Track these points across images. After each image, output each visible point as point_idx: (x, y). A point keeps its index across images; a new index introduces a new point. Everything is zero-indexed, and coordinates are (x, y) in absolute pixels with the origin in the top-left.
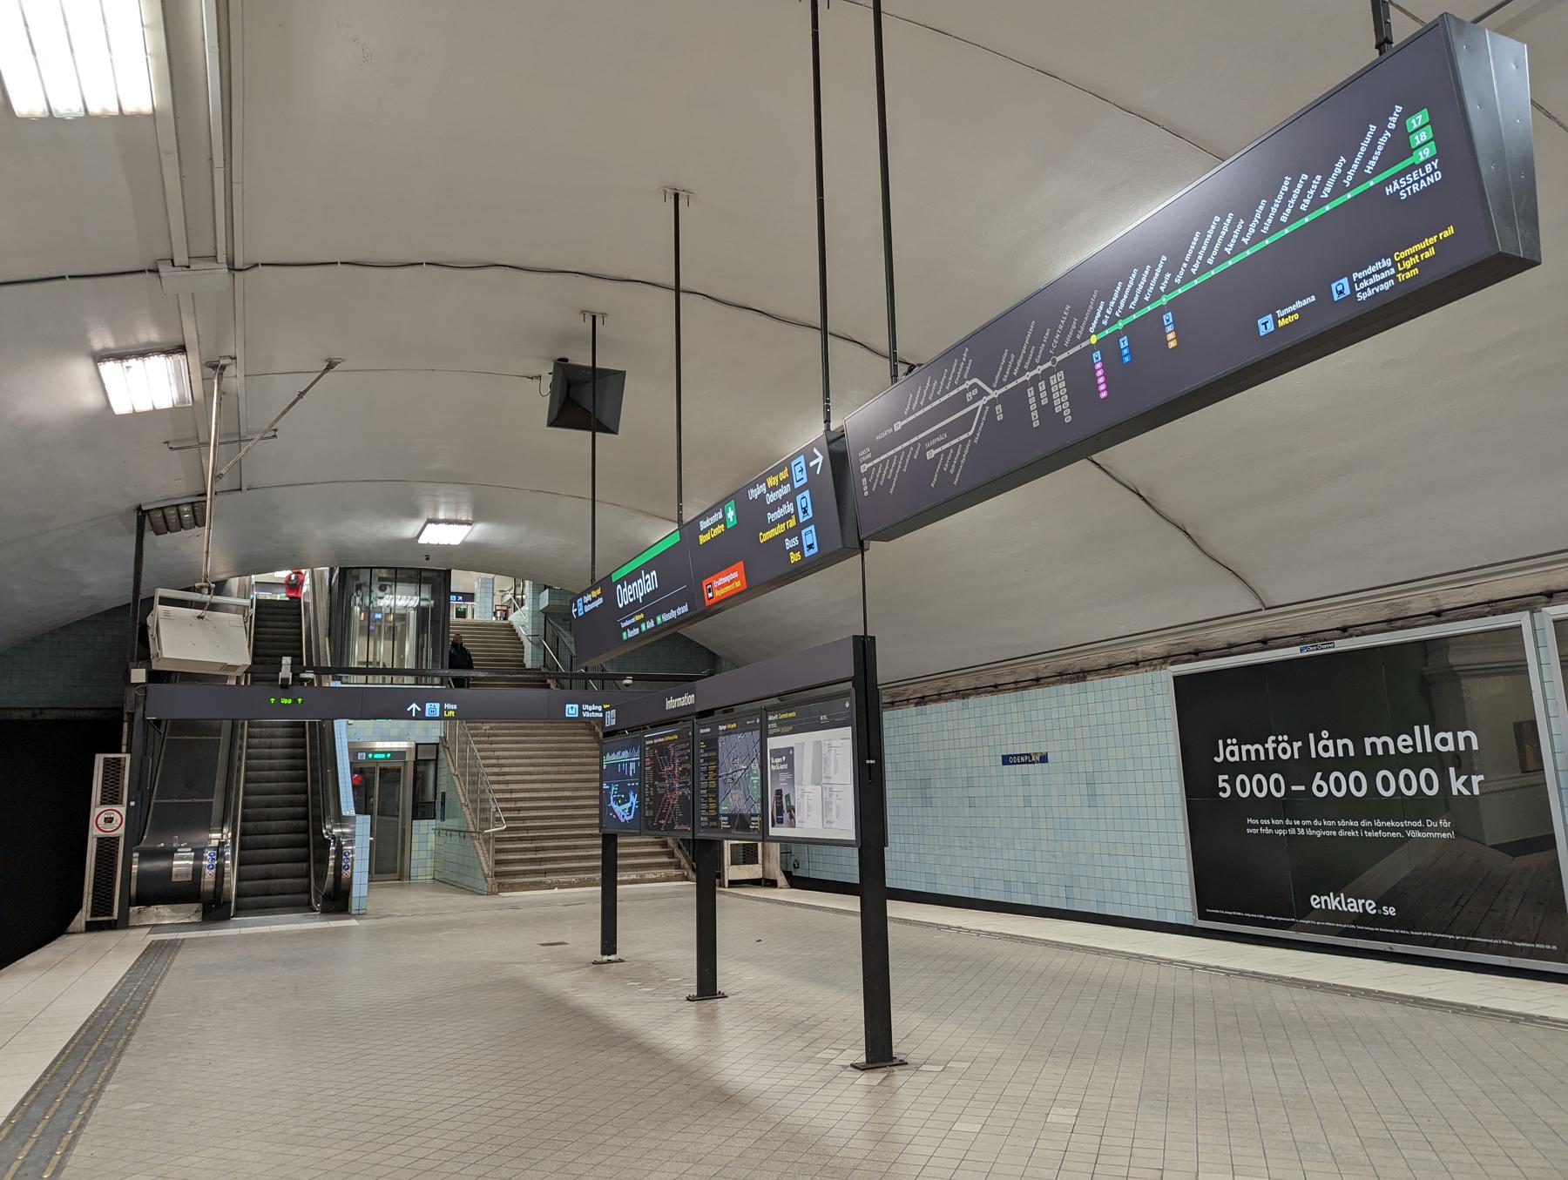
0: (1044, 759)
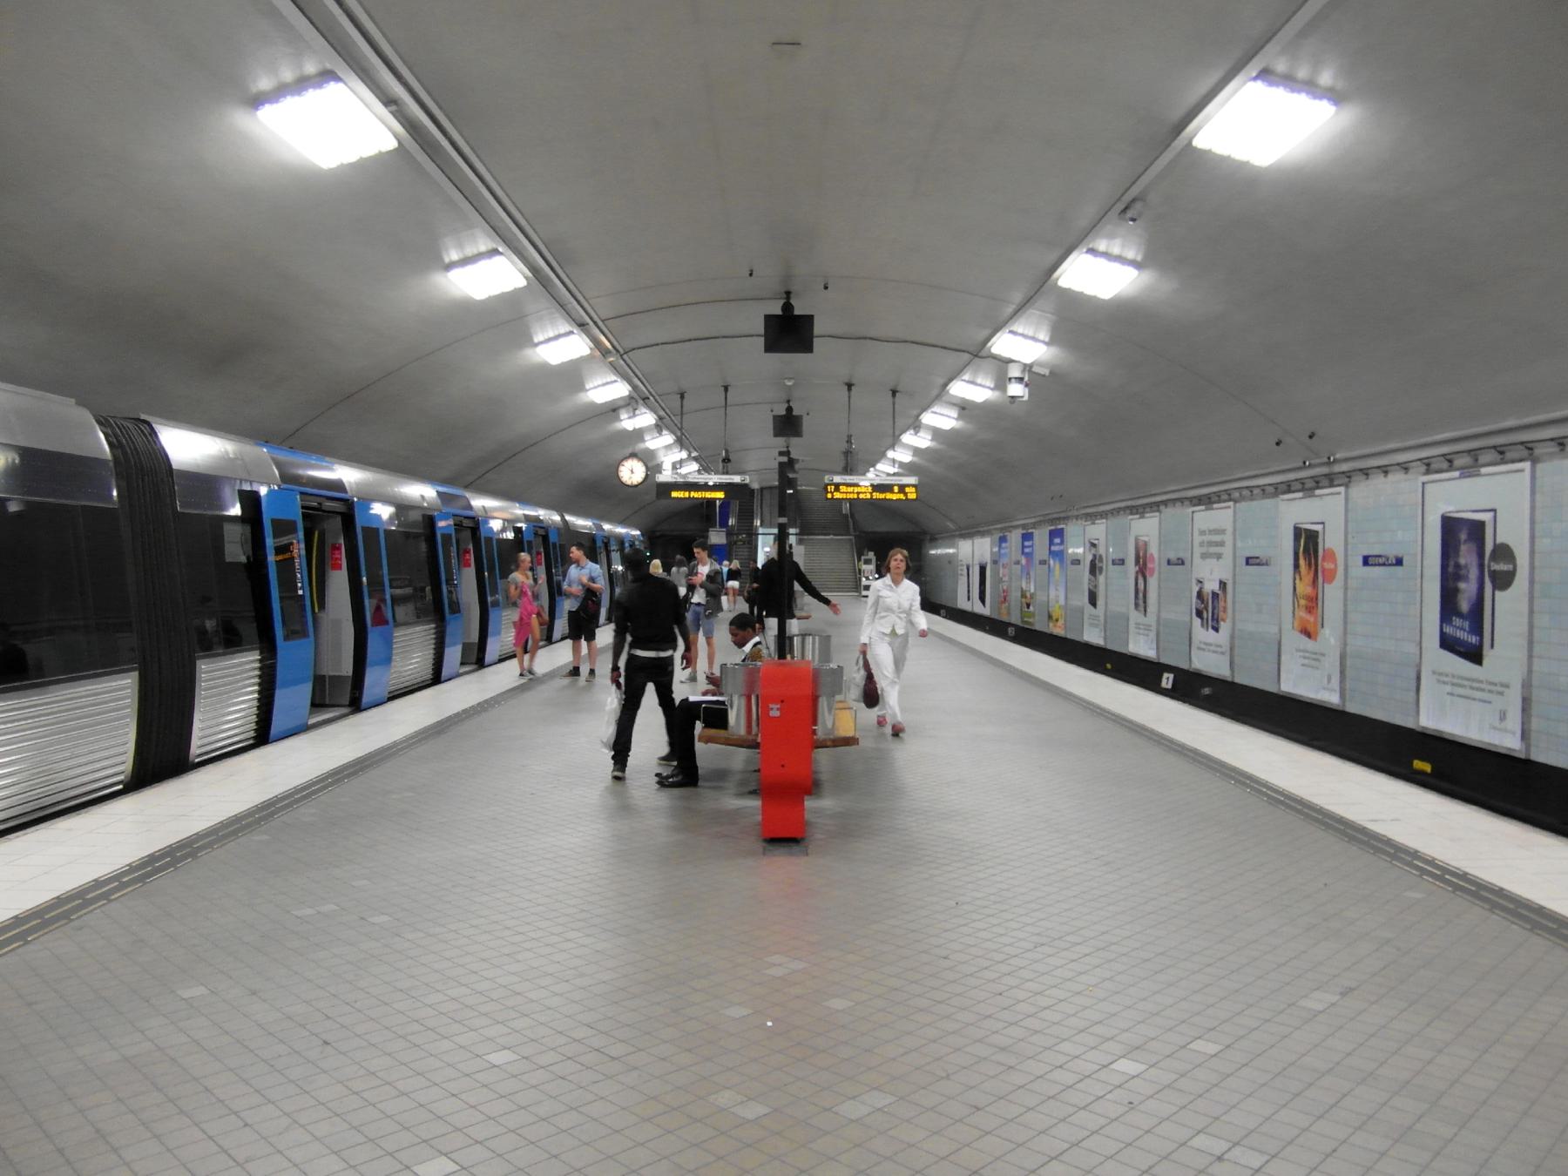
0: (1399, 562)
